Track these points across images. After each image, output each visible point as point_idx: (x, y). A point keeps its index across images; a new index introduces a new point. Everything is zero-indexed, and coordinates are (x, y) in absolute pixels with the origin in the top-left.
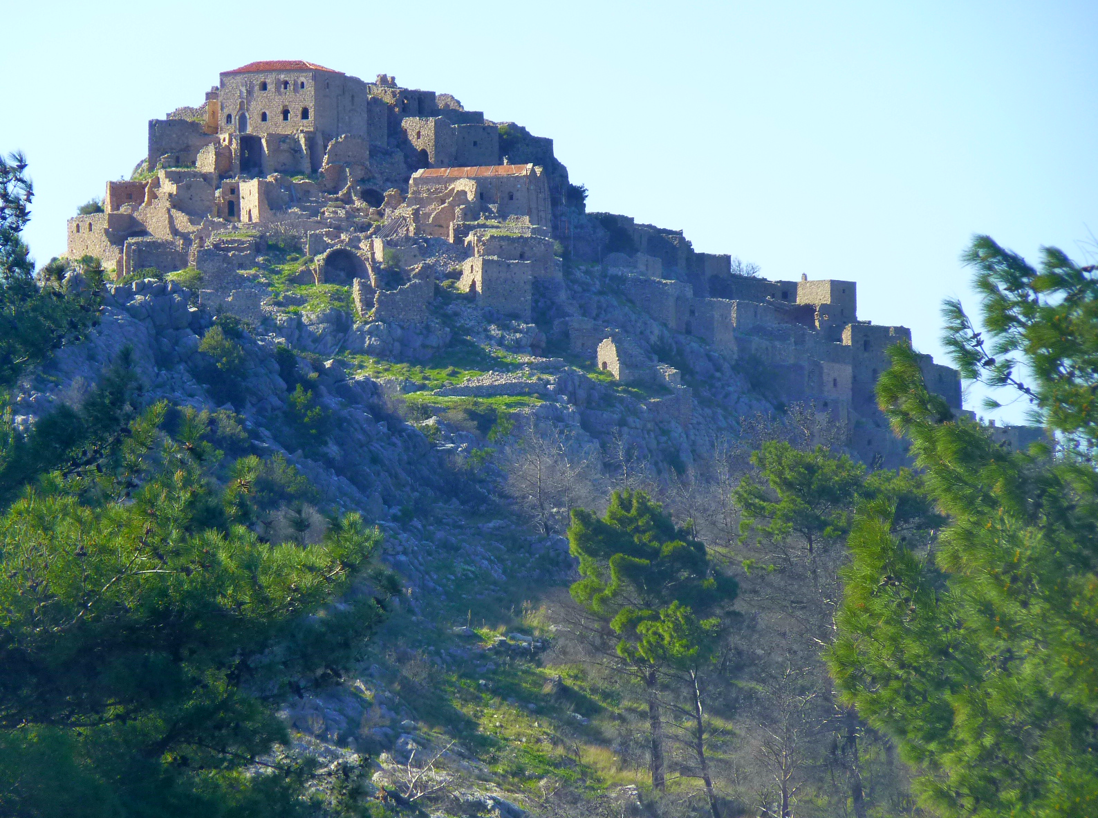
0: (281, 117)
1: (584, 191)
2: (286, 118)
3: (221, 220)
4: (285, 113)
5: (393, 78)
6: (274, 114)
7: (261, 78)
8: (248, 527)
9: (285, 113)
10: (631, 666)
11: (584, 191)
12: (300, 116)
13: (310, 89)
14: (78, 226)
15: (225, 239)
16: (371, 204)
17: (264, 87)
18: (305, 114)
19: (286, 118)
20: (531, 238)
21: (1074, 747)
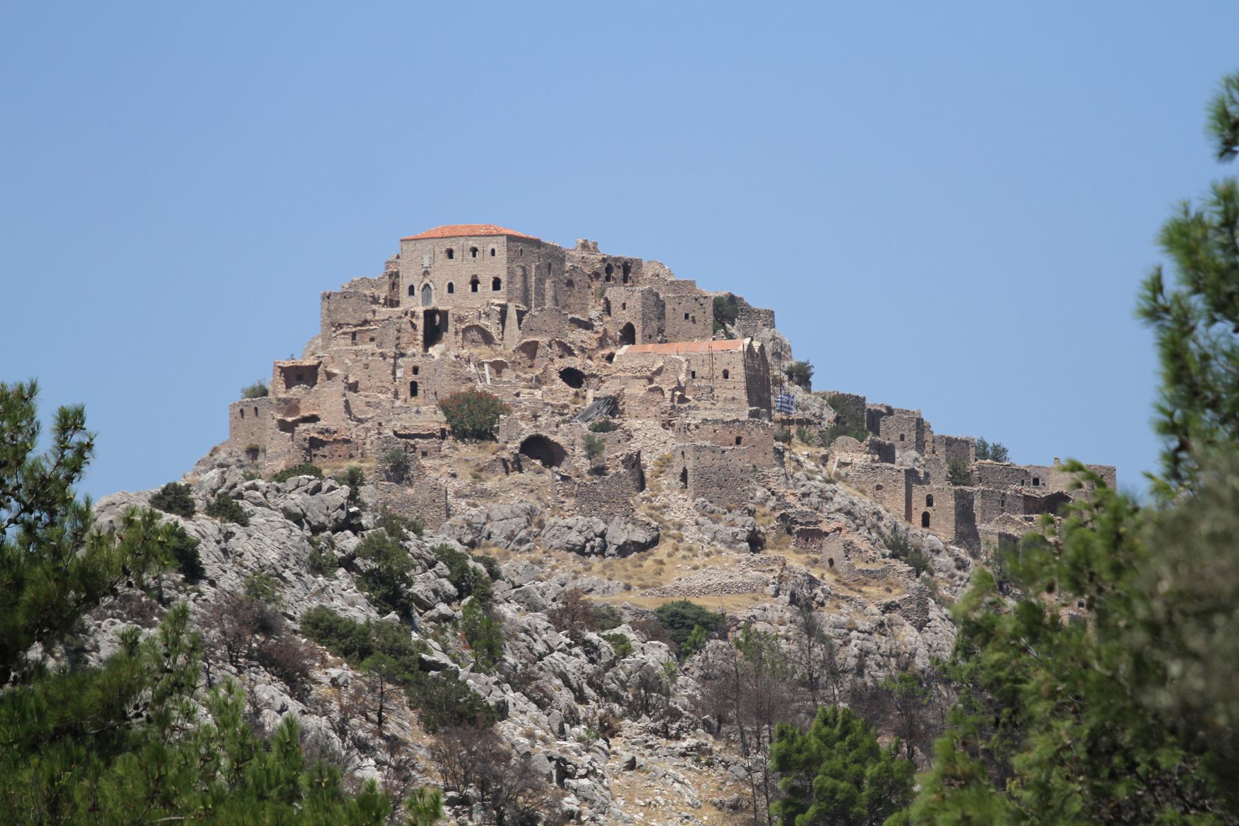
0: (470, 287)
1: (809, 368)
2: (475, 289)
3: (988, 461)
4: (475, 283)
5: (595, 244)
6: (463, 286)
7: (472, 243)
8: (91, 601)
9: (475, 283)
10: (571, 747)
11: (809, 368)
12: (491, 287)
13: (502, 255)
14: (242, 411)
15: (407, 425)
16: (571, 384)
17: (450, 254)
18: (497, 284)
19: (475, 289)
20: (748, 422)
21: (335, 655)
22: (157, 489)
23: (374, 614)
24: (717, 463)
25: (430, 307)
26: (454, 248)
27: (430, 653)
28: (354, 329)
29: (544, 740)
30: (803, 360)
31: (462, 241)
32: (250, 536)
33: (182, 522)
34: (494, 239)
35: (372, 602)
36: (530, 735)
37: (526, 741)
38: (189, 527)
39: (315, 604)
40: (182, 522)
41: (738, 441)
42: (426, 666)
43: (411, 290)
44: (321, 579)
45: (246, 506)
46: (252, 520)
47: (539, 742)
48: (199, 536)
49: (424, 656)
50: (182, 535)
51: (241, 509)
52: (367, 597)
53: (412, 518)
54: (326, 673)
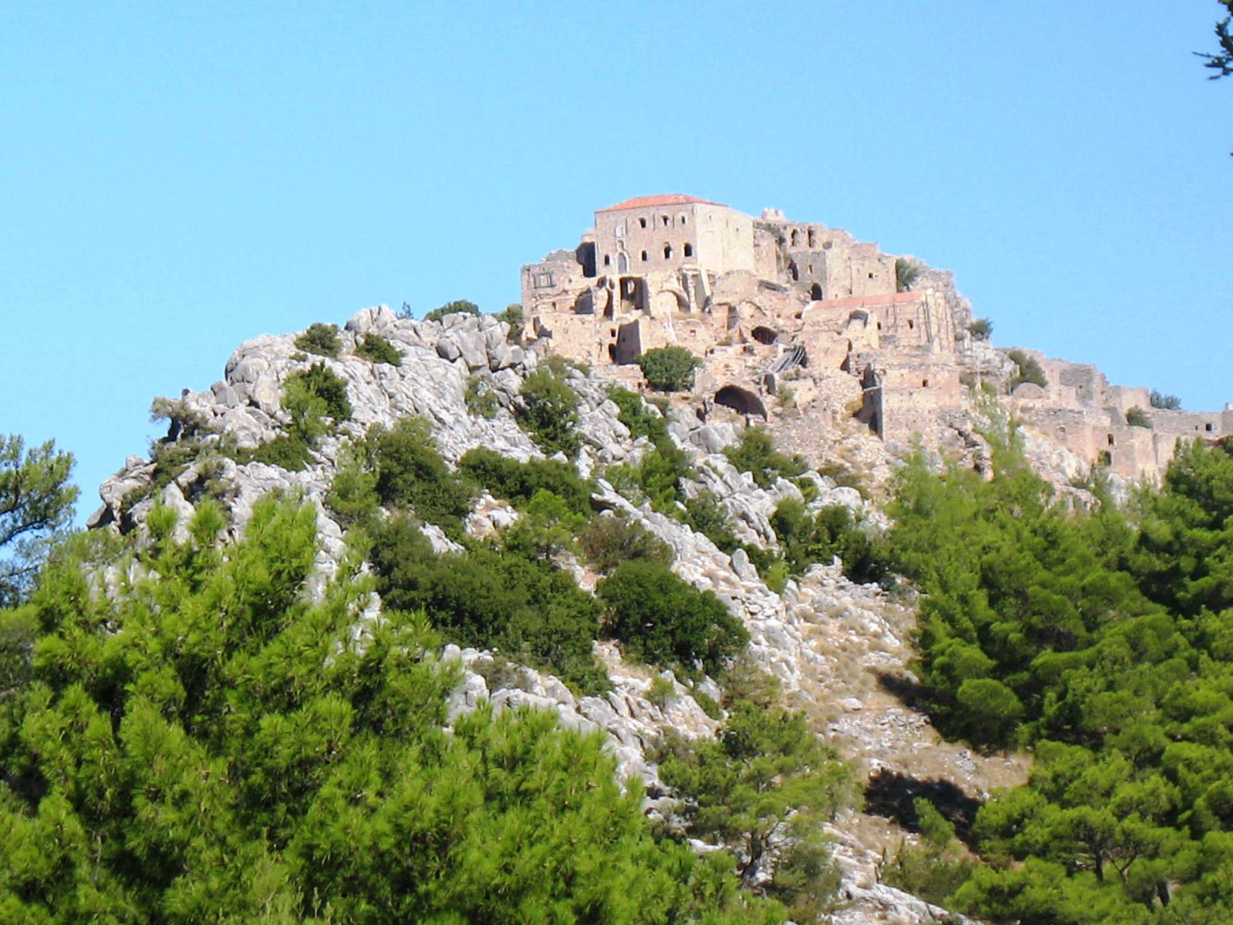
2: (667, 256)
6: (656, 253)
19: (667, 256)
22: (302, 332)
23: (540, 455)
24: (905, 405)
25: (626, 275)
26: (646, 218)
27: (601, 493)
28: (553, 300)
29: (726, 580)
30: (984, 318)
31: (653, 211)
32: (403, 376)
33: (328, 362)
34: (684, 207)
35: (536, 441)
36: (710, 575)
37: (708, 581)
38: (337, 369)
39: (475, 445)
40: (328, 362)
41: (925, 383)
42: (600, 506)
43: (607, 261)
44: (481, 420)
45: (398, 346)
46: (404, 360)
47: (722, 583)
48: (347, 376)
49: (594, 496)
50: (328, 376)
51: (393, 348)
52: (531, 438)
53: (579, 360)
54: (489, 516)
